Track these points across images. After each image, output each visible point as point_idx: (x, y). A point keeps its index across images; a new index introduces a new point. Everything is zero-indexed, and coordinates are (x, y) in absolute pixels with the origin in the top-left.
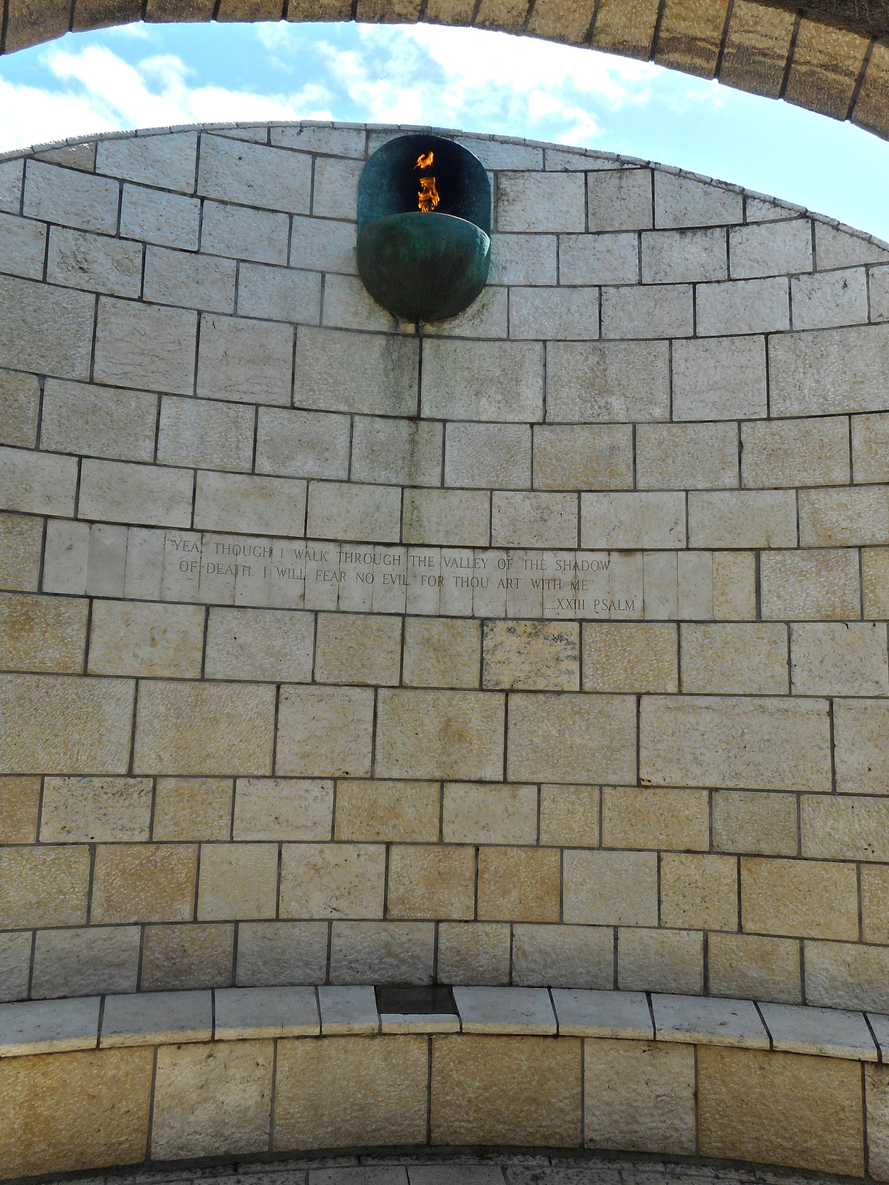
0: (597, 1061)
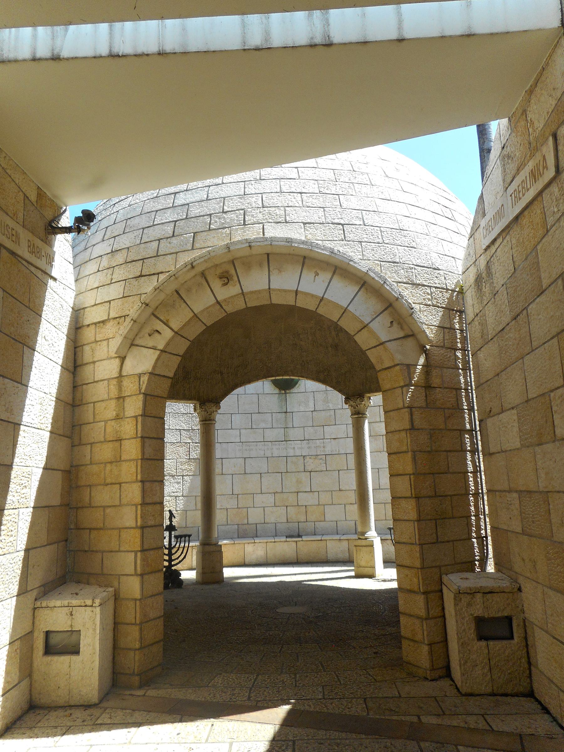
0: (329, 544)
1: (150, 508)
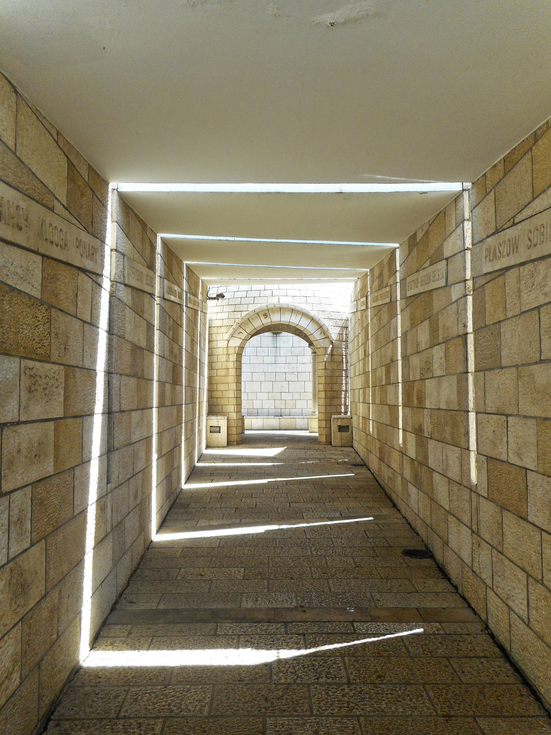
1: (238, 391)
